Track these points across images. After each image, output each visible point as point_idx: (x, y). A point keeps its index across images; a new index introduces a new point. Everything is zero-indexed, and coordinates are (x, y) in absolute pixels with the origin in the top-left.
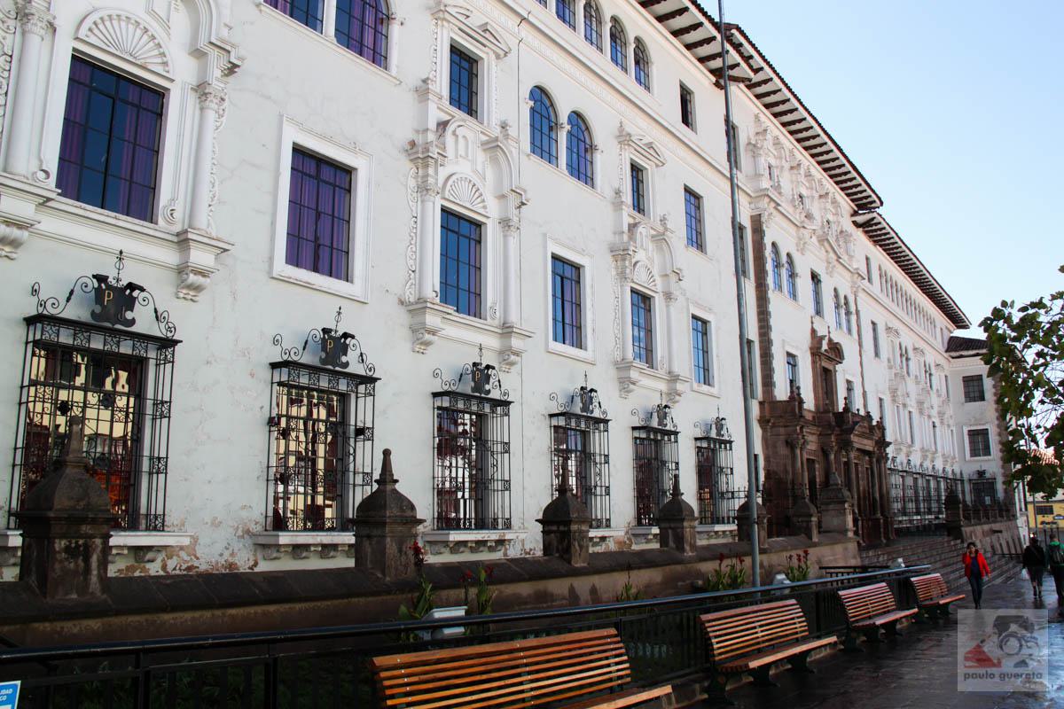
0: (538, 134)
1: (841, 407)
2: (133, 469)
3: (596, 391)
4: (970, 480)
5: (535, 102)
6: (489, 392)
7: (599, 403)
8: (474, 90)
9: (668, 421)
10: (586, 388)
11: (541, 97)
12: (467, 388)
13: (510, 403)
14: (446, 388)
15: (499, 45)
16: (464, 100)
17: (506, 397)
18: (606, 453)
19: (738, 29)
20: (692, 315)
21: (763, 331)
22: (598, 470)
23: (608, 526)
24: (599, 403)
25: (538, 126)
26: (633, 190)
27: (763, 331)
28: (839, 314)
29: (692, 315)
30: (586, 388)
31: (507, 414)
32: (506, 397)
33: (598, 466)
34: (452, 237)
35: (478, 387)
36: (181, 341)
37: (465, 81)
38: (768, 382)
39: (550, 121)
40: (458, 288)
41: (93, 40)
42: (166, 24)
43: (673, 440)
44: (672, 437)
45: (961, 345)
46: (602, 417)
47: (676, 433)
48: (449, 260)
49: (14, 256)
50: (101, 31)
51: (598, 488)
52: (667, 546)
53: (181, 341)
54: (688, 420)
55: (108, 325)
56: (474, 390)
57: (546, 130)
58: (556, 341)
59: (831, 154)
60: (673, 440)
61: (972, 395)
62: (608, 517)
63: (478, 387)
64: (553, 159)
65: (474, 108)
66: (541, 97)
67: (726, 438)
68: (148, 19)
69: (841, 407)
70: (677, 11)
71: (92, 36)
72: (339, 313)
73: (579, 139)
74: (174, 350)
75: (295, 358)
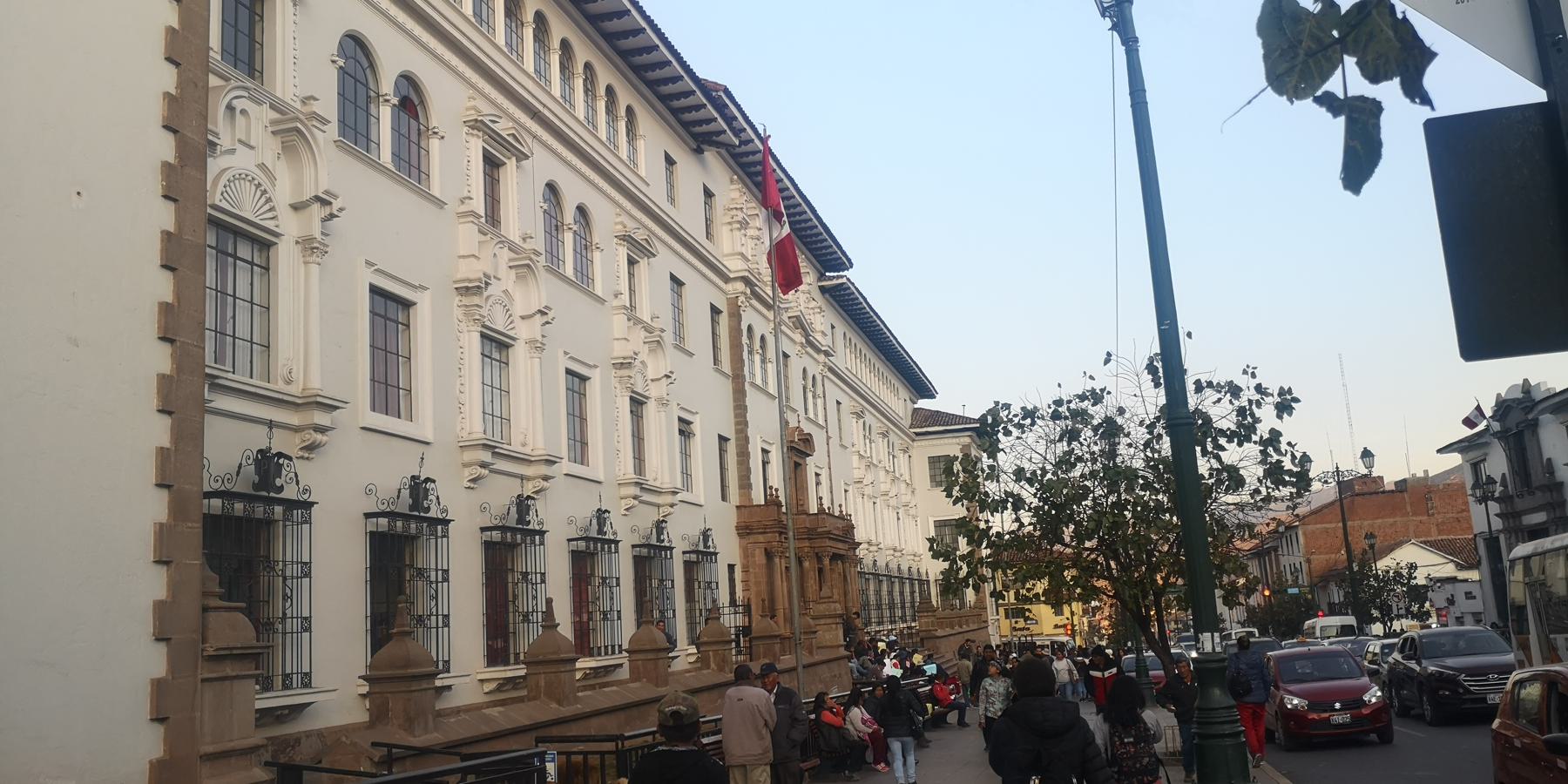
0: (350, 107)
1: (814, 509)
2: (440, 630)
3: (434, 481)
4: (936, 581)
5: (347, 59)
6: (281, 489)
7: (438, 498)
8: (258, 39)
9: (710, 543)
10: (419, 477)
11: (356, 47)
12: (404, 505)
13: (312, 504)
14: (496, 522)
15: (519, 147)
16: (243, 54)
17: (444, 515)
18: (445, 567)
19: (726, 91)
20: (567, 369)
21: (740, 427)
22: (433, 592)
23: (308, 685)
24: (611, 523)
25: (350, 94)
26: (575, 250)
27: (740, 427)
28: (766, 371)
29: (567, 369)
30: (419, 477)
31: (308, 521)
32: (306, 497)
33: (434, 586)
34: (582, 392)
35: (522, 519)
36: (317, 503)
37: (244, 25)
38: (745, 484)
39: (368, 88)
40: (386, 383)
41: (224, 205)
42: (272, 178)
43: (537, 542)
44: (537, 537)
45: (926, 421)
46: (440, 517)
47: (446, 522)
48: (249, 300)
49: (311, 456)
50: (261, 207)
51: (434, 618)
52: (709, 668)
53: (317, 503)
54: (681, 534)
55: (265, 494)
56: (412, 508)
57: (414, 137)
58: (374, 411)
59: (792, 200)
60: (537, 542)
61: (938, 479)
62: (446, 658)
63: (522, 519)
64: (414, 172)
65: (258, 67)
66: (356, 47)
67: (610, 536)
68: (257, 171)
69: (814, 509)
70: (706, 120)
71: (224, 201)
72: (422, 459)
73: (356, 80)
74: (310, 513)
75: (229, 486)
